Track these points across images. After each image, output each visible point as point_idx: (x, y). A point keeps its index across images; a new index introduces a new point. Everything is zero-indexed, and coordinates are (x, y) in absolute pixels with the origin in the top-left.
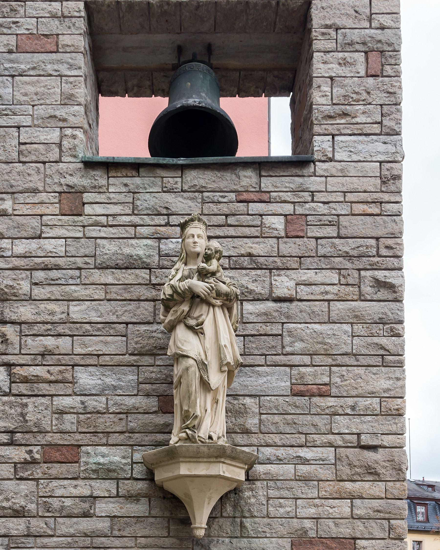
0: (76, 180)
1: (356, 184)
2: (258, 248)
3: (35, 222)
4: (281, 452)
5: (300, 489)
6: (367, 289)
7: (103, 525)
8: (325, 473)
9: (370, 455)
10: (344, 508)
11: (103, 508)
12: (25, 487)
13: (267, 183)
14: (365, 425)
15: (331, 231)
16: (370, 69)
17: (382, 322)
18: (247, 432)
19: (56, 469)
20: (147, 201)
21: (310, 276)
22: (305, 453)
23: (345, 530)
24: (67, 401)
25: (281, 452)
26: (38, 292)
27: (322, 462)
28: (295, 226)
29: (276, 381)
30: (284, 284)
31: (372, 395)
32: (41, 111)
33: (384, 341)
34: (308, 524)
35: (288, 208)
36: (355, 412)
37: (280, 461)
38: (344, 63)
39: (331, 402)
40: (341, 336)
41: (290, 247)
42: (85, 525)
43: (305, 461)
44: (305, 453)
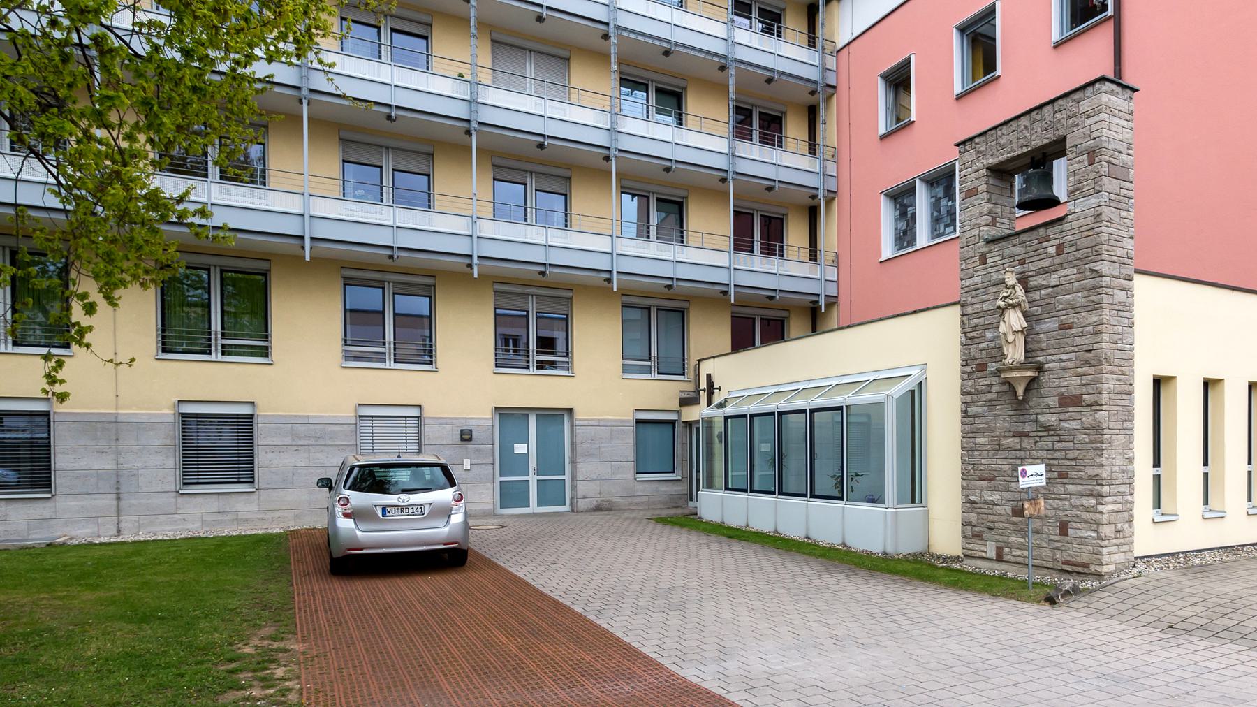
0: (983, 250)
1: (1083, 222)
2: (1045, 264)
3: (971, 271)
4: (1054, 358)
5: (1062, 374)
6: (1088, 273)
7: (994, 396)
8: (1071, 365)
9: (1089, 355)
10: (1078, 380)
11: (995, 389)
12: (971, 382)
13: (1049, 232)
14: (1087, 339)
15: (1073, 248)
16: (413, 474)
17: (1094, 288)
18: (658, 315)
19: (980, 374)
20: (1007, 252)
21: (1065, 272)
22: (1063, 357)
23: (1078, 392)
24: (983, 345)
25: (1054, 358)
26: (974, 300)
27: (1070, 360)
28: (1060, 249)
29: (1051, 324)
30: (1054, 279)
31: (1089, 325)
32: (973, 222)
33: (1094, 298)
34: (1063, 390)
35: (1057, 242)
36: (1084, 334)
37: (1054, 362)
38: (1079, 162)
39: (1073, 331)
40: (1079, 299)
41: (1058, 260)
42: (989, 396)
43: (1063, 361)
44: (1063, 357)
